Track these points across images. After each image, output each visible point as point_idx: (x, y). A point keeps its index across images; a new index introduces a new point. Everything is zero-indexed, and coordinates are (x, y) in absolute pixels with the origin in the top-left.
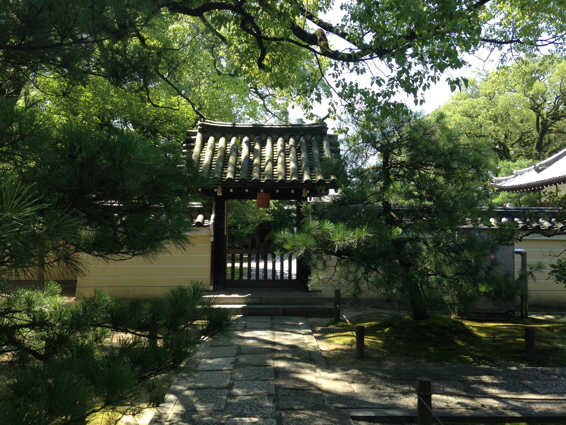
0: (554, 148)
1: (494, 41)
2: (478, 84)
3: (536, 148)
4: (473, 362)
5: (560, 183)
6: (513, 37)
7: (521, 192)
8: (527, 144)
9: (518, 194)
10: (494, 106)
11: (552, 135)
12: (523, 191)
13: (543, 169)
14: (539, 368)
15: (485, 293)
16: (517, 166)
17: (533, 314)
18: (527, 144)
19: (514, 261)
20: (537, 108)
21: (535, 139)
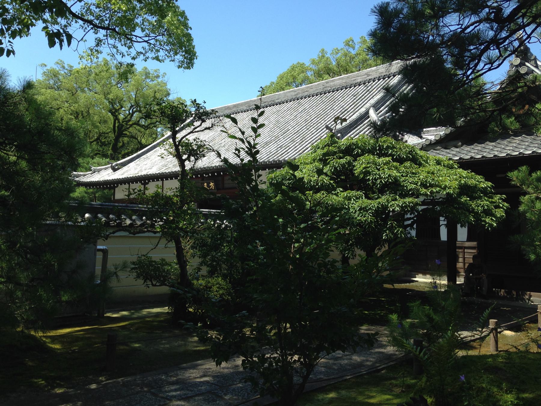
0: (126, 151)
1: (90, 22)
2: (60, 77)
3: (112, 149)
4: (46, 386)
5: (133, 183)
6: (109, 24)
7: (98, 188)
8: (103, 144)
9: (95, 190)
10: (76, 102)
11: (126, 139)
12: (100, 187)
13: (118, 169)
14: (120, 379)
15: (67, 302)
16: (95, 163)
17: (109, 312)
18: (103, 144)
19: (95, 258)
20: (114, 113)
21: (111, 140)
